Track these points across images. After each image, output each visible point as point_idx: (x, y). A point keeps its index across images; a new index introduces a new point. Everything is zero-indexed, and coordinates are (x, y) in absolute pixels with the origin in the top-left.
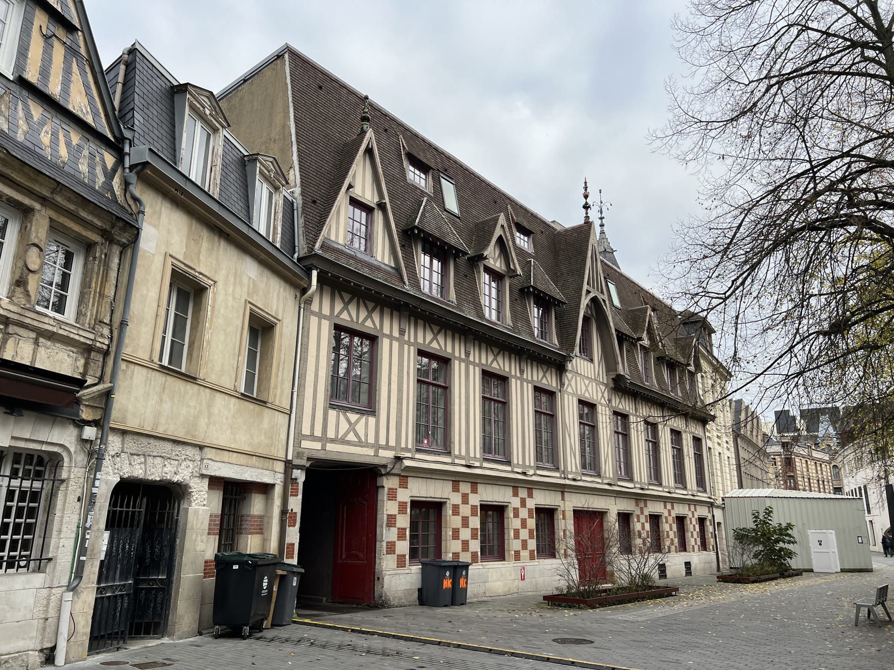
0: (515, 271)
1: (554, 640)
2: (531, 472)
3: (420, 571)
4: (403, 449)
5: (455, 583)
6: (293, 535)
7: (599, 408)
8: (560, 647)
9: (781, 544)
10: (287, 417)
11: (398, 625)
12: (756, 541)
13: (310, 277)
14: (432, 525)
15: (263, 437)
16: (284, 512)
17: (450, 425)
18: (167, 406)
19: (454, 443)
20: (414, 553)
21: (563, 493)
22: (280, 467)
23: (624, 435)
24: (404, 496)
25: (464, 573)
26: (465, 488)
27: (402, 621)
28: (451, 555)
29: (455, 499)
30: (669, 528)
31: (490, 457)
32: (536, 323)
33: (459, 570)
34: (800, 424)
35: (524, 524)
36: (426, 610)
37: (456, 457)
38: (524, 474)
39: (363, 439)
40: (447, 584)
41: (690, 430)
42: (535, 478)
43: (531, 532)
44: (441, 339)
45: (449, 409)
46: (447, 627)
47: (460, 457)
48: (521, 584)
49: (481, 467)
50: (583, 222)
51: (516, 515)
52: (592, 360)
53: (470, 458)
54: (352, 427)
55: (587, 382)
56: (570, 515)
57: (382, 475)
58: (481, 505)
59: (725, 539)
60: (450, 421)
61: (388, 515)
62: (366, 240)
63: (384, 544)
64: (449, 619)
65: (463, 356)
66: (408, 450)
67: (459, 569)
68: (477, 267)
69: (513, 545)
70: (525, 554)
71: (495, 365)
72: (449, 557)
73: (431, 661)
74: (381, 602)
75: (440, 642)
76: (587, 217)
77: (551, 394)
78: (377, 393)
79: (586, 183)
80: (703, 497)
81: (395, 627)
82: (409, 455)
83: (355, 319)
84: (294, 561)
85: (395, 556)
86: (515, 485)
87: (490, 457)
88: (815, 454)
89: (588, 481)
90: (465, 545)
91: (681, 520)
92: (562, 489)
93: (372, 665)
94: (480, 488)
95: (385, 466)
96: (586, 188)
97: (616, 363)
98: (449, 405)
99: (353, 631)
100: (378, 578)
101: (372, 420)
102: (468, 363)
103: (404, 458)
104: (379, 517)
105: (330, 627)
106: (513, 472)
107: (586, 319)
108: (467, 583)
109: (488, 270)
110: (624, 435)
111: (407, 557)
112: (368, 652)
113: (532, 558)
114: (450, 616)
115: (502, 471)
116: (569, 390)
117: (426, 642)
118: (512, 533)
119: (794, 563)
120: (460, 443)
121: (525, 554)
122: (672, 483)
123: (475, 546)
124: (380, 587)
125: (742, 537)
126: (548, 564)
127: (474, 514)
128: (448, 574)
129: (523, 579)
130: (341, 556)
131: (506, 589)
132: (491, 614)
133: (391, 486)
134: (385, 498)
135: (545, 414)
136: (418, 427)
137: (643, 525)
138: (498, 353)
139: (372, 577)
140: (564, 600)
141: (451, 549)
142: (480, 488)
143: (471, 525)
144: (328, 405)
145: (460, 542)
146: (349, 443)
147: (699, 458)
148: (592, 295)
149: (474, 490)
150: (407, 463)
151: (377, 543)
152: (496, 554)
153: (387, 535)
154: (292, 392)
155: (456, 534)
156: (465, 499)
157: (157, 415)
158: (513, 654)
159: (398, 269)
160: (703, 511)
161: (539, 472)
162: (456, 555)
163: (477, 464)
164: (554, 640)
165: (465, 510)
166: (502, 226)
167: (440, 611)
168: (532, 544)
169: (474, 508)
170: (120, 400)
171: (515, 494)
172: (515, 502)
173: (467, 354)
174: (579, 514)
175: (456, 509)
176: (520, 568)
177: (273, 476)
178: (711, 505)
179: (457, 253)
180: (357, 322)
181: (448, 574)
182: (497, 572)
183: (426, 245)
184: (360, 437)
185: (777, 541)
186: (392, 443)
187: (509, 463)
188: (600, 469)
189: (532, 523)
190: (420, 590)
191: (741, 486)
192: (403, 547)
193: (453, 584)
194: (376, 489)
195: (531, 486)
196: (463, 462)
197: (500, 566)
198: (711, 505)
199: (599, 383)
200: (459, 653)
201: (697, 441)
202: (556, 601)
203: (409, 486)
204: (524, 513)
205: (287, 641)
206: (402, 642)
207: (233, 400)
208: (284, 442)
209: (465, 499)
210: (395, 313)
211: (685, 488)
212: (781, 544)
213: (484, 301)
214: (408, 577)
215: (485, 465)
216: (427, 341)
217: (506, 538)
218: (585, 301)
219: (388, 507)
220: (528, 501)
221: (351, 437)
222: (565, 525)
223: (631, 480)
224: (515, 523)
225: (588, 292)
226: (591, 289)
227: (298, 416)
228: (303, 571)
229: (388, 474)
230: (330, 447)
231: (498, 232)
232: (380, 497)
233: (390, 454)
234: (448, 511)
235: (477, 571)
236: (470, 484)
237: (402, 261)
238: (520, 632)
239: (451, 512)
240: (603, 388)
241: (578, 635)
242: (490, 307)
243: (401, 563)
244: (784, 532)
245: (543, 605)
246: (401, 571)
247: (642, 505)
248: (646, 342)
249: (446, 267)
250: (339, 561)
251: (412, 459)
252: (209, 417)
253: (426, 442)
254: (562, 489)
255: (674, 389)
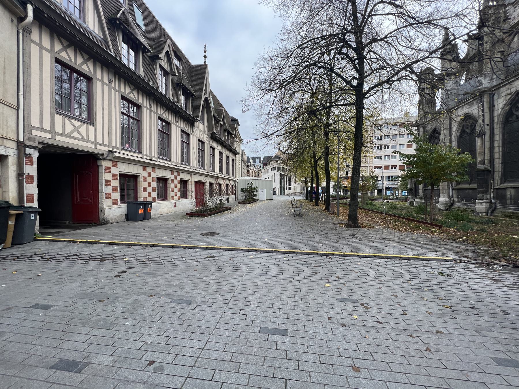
0: (174, 72)
1: (201, 234)
2: (179, 165)
3: (126, 206)
4: (113, 147)
5: (145, 210)
6: (32, 189)
7: (205, 144)
8: (206, 238)
9: (254, 193)
10: (15, 112)
11: (114, 234)
12: (248, 191)
13: (25, 9)
14: (132, 186)
16: (20, 175)
17: (141, 140)
19: (143, 148)
20: (122, 199)
21: (191, 174)
23: (213, 156)
24: (116, 171)
25: (150, 206)
27: (116, 231)
28: (142, 199)
30: (223, 188)
31: (161, 157)
32: (183, 102)
33: (147, 205)
34: (251, 161)
35: (176, 186)
36: (130, 224)
37: (144, 155)
38: (176, 166)
39: (85, 137)
40: (141, 211)
41: (232, 157)
42: (180, 168)
43: (178, 189)
44: (135, 93)
45: (140, 132)
46: (143, 233)
47: (146, 155)
48: (175, 209)
50: (203, 64)
51: (173, 182)
52: (204, 124)
53: (151, 157)
54: (76, 129)
55: (202, 133)
56: (193, 183)
57: (100, 159)
58: (157, 178)
59: (239, 190)
60: (141, 137)
61: (106, 180)
62: (80, 11)
63: (104, 194)
64: (143, 228)
65: (148, 106)
66: (118, 148)
67: (147, 205)
68: (155, 63)
69: (171, 194)
70: (176, 197)
71: (164, 115)
72: (142, 199)
73: (138, 261)
74: (103, 222)
75: (141, 244)
76: (205, 62)
77: (188, 135)
78: (94, 113)
79: (205, 45)
80: (233, 178)
81: (112, 236)
82: (118, 151)
83: (73, 60)
84: (35, 204)
85: (111, 200)
86: (172, 170)
87: (161, 157)
88: (255, 169)
89: (200, 171)
90: (150, 194)
91: (227, 185)
92: (191, 173)
93: (89, 273)
94: (157, 170)
95: (102, 155)
96: (205, 48)
97: (213, 127)
98: (140, 130)
99: (81, 242)
100: (101, 211)
101: (91, 128)
102: (151, 111)
103: (115, 152)
104: (100, 180)
105: (64, 241)
106: (171, 164)
107: (203, 107)
108: (151, 210)
109: (162, 68)
110: (213, 156)
111: (119, 200)
112: (89, 259)
113: (179, 199)
114: (144, 226)
115: (167, 164)
116: (195, 134)
117: (132, 245)
118: (171, 190)
119: (256, 198)
120: (147, 149)
121: (176, 197)
122: (226, 174)
123: (154, 195)
124: (103, 214)
125: (243, 191)
126: (184, 201)
127: (154, 181)
128: (141, 207)
129: (175, 207)
130: (77, 200)
131: (168, 211)
132: (164, 223)
133: (107, 165)
134: (103, 172)
135: (185, 142)
136: (123, 138)
138: (166, 111)
139: (97, 210)
140: (195, 214)
141: (142, 196)
142: (157, 170)
143: (152, 186)
144: (54, 111)
145: (147, 193)
146: (74, 138)
147: (233, 166)
148: (206, 96)
149: (154, 171)
150: (116, 154)
151: (100, 194)
152: (163, 198)
153: (105, 190)
154: (18, 95)
155: (145, 190)
156: (149, 174)
158: (186, 247)
159: (106, 41)
160: (233, 183)
161: (182, 166)
162: (144, 198)
163: (155, 159)
164: (201, 234)
165: (149, 179)
166: (169, 46)
167: (138, 224)
168: (179, 194)
169: (153, 179)
171: (172, 174)
172: (172, 177)
173: (150, 106)
174: (196, 183)
175: (145, 179)
178: (235, 181)
179: (145, 50)
180: (76, 63)
181: (141, 207)
183: (125, 36)
184: (83, 136)
185: (253, 192)
186: (106, 142)
187: (170, 161)
188: (204, 166)
189: (179, 186)
190: (126, 215)
191: (242, 176)
192: (116, 195)
193: (144, 211)
194: (97, 167)
195: (179, 171)
196: (149, 158)
198: (235, 181)
199: (206, 134)
200: (155, 250)
201: (233, 160)
202: (191, 215)
203: (118, 166)
204: (176, 182)
205: (18, 258)
206: (116, 247)
208: (15, 129)
209: (149, 174)
210: (104, 68)
211: (229, 175)
212: (254, 193)
213: (160, 83)
214: (120, 210)
215: (159, 160)
216: (127, 92)
217: (168, 191)
218: (203, 98)
219: (104, 176)
220: (178, 177)
221: (75, 134)
222: (192, 187)
223: (214, 172)
224: (173, 186)
225: (205, 95)
226: (206, 93)
227: (26, 112)
228: (40, 210)
229: (104, 159)
230: (58, 138)
231: (166, 49)
232: (100, 171)
233: (106, 149)
234: (141, 179)
237: (108, 36)
238: (183, 232)
239: (142, 180)
240: (207, 136)
241: (209, 230)
242: (162, 87)
243: (115, 202)
244: (255, 189)
245: (186, 217)
246: (115, 206)
247: (217, 180)
248: (221, 123)
249: (138, 58)
250: (75, 203)
251: (119, 153)
253: (128, 146)
254: (191, 173)
255: (228, 141)
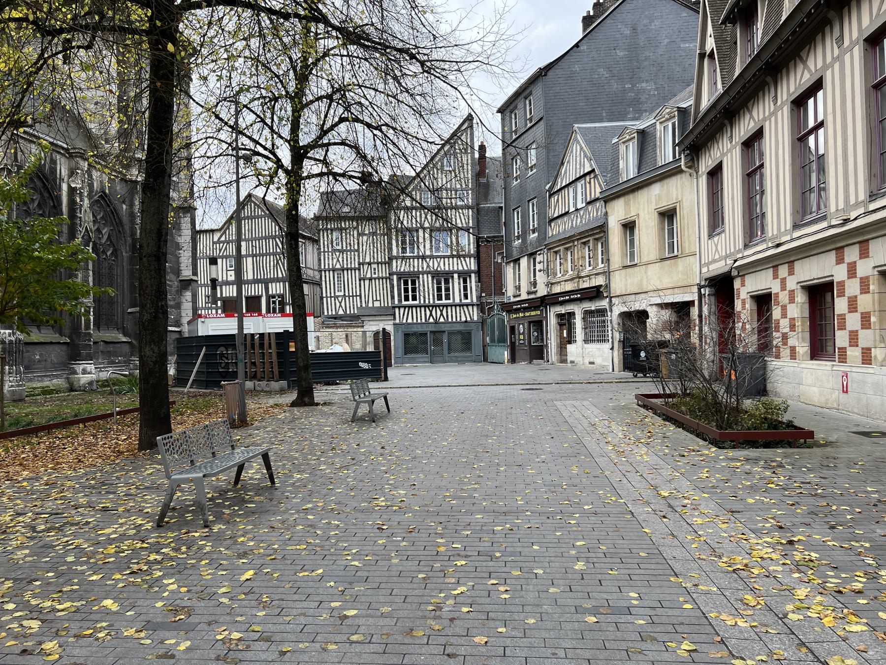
15: (680, 276)
18: (629, 281)
22: (695, 289)
26: (783, 271)
29: (839, 273)
49: (792, 240)
137: (784, 315)
157: (626, 286)
170: (613, 285)
171: (840, 260)
176: (841, 374)
177: (691, 296)
182: (812, 374)
197: (814, 367)
207: (657, 264)
235: (792, 369)
236: (772, 269)
252: (647, 278)
